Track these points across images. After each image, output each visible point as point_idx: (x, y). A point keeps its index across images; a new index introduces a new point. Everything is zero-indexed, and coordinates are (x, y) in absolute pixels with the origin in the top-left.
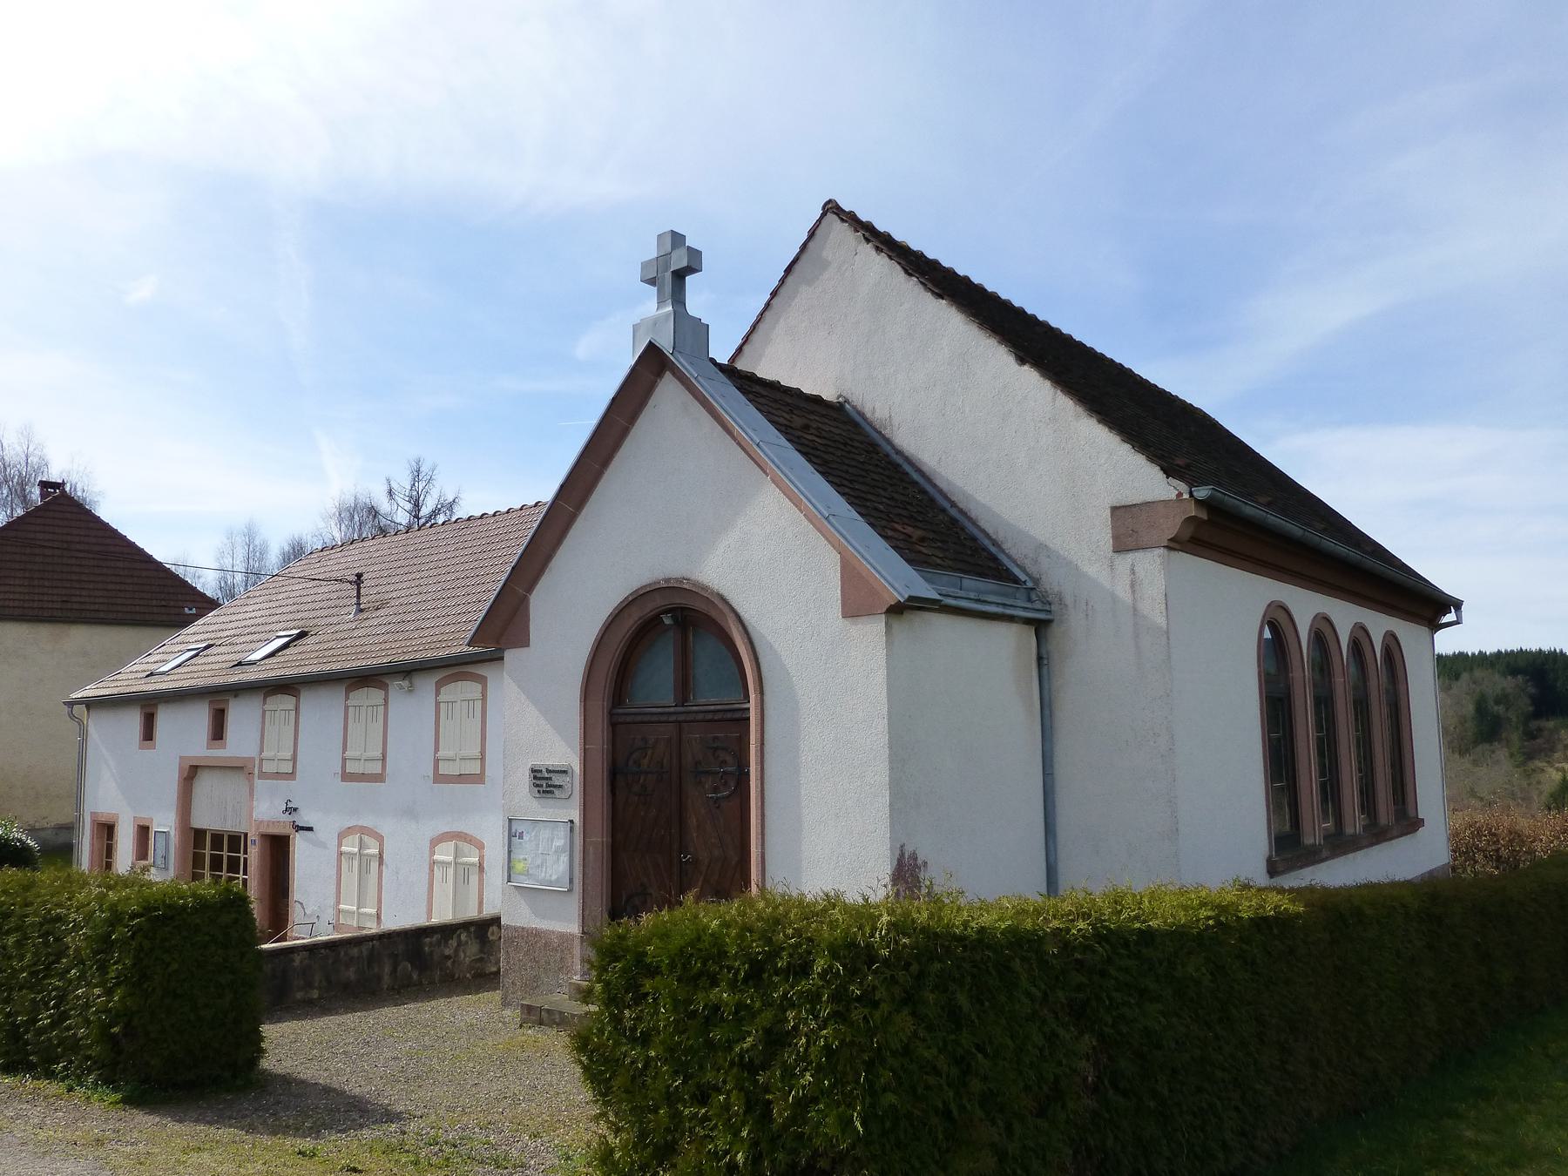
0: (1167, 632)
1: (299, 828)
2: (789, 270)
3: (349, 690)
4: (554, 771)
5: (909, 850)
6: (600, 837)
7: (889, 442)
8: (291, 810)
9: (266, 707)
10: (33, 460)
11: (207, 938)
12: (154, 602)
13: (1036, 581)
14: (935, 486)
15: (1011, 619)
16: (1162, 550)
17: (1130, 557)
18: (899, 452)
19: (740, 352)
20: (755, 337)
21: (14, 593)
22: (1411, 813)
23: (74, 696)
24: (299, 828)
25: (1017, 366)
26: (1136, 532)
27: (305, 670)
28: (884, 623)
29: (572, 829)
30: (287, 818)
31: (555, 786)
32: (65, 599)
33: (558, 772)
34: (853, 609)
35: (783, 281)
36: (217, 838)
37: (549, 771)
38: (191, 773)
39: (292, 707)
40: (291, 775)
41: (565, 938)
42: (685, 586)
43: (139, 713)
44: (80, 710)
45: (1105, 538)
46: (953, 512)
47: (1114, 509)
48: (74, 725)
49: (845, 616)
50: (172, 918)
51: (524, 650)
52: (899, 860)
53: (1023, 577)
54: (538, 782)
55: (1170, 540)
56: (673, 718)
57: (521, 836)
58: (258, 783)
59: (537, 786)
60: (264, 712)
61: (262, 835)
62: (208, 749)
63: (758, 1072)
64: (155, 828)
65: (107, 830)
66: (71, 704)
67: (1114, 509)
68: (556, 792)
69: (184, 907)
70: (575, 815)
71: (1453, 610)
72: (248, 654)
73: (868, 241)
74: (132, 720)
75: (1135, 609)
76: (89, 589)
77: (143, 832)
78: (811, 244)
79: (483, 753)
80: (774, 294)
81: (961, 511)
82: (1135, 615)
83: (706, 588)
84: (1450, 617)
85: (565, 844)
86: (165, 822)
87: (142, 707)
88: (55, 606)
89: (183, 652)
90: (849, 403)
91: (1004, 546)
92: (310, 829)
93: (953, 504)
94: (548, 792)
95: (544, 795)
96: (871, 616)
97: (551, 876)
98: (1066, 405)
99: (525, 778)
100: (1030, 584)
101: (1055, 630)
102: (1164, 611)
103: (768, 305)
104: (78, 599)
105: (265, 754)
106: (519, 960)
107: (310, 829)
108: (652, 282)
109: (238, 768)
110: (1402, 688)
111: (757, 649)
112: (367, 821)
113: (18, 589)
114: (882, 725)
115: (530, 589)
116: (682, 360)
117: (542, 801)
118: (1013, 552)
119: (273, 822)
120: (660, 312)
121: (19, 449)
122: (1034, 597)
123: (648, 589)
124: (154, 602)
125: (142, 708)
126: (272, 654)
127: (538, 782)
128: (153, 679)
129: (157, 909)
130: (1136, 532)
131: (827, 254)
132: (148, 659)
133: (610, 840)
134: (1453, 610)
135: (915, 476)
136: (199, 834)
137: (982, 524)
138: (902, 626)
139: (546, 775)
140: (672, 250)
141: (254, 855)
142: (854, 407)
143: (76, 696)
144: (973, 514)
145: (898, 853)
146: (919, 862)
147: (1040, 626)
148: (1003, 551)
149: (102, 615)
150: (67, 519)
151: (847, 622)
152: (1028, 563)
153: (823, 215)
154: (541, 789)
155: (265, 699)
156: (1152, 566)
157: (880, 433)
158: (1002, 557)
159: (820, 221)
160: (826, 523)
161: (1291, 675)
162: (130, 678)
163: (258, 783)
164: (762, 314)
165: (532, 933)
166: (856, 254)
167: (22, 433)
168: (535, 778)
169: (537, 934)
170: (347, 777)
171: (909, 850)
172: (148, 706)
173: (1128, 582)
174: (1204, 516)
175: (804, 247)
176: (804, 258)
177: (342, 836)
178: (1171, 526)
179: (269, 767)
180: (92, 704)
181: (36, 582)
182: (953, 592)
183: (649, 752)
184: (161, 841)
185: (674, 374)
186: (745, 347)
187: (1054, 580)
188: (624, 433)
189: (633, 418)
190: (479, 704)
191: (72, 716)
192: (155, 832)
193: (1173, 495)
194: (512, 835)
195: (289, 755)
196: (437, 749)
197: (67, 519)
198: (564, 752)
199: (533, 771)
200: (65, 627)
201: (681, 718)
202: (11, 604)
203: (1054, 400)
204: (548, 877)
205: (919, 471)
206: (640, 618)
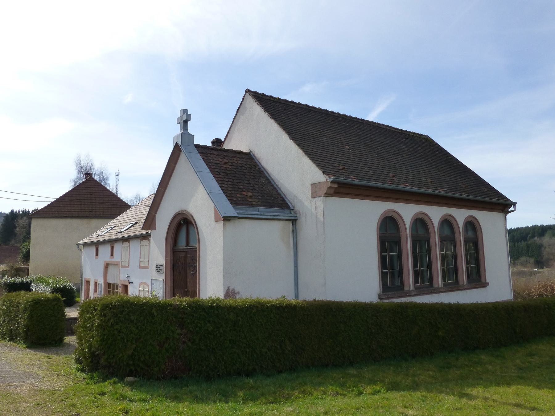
0: (324, 223)
1: (130, 283)
2: (238, 111)
3: (141, 240)
5: (231, 288)
6: (170, 284)
7: (260, 164)
8: (128, 277)
9: (141, 244)
10: (90, 164)
11: (48, 308)
12: (117, 211)
13: (294, 207)
14: (271, 177)
15: (280, 220)
16: (322, 197)
17: (315, 199)
18: (263, 167)
20: (230, 132)
21: (76, 209)
22: (483, 280)
23: (79, 243)
24: (130, 283)
27: (132, 234)
28: (223, 224)
29: (163, 282)
30: (127, 279)
31: (160, 270)
32: (91, 211)
34: (217, 220)
35: (236, 114)
36: (113, 285)
38: (107, 266)
39: (128, 246)
40: (128, 267)
43: (94, 248)
44: (81, 247)
45: (309, 193)
46: (275, 186)
47: (312, 184)
48: (79, 252)
50: (39, 302)
52: (227, 291)
53: (291, 206)
54: (157, 269)
55: (325, 194)
56: (185, 250)
58: (121, 268)
60: (140, 246)
61: (122, 285)
62: (110, 258)
64: (99, 283)
65: (88, 283)
66: (78, 245)
67: (312, 184)
69: (43, 300)
71: (513, 206)
72: (121, 229)
73: (256, 102)
74: (93, 249)
76: (98, 207)
77: (96, 283)
78: (243, 103)
79: (129, 260)
80: (234, 118)
81: (277, 185)
82: (316, 218)
83: (188, 213)
84: (512, 209)
86: (101, 281)
87: (96, 246)
88: (88, 213)
89: (108, 228)
90: (251, 152)
91: (287, 196)
92: (132, 283)
93: (275, 183)
98: (300, 152)
99: (154, 268)
100: (292, 208)
101: (298, 222)
102: (323, 216)
103: (233, 121)
104: (95, 211)
105: (123, 260)
107: (132, 283)
108: (179, 123)
109: (116, 264)
110: (479, 235)
111: (199, 231)
112: (144, 281)
113: (77, 208)
114: (222, 253)
115: (156, 213)
116: (182, 147)
118: (288, 198)
119: (125, 281)
121: (85, 162)
122: (292, 212)
124: (117, 211)
126: (127, 229)
127: (157, 269)
128: (99, 237)
129: (35, 300)
131: (247, 105)
132: (100, 231)
133: (173, 285)
134: (513, 206)
135: (267, 175)
136: (109, 284)
137: (281, 189)
138: (227, 223)
139: (159, 267)
140: (183, 114)
141: (120, 289)
142: (253, 153)
143: (80, 243)
144: (280, 186)
145: (226, 289)
146: (236, 292)
147: (294, 221)
148: (286, 198)
149: (102, 215)
150: (92, 185)
151: (216, 223)
152: (292, 201)
153: (246, 93)
155: (122, 243)
156: (319, 201)
157: (258, 161)
158: (286, 200)
159: (245, 95)
161: (401, 233)
162: (93, 238)
163: (121, 268)
164: (232, 125)
167: (86, 156)
168: (157, 267)
170: (141, 267)
171: (231, 288)
172: (97, 245)
173: (315, 207)
174: (336, 186)
175: (241, 103)
176: (241, 107)
177: (140, 285)
178: (324, 190)
179: (123, 264)
180: (84, 245)
181: (82, 206)
182: (250, 213)
183: (180, 260)
184: (100, 286)
186: (228, 135)
187: (298, 207)
190: (128, 247)
191: (79, 249)
192: (99, 284)
194: (152, 284)
195: (127, 260)
196: (140, 259)
197: (92, 185)
198: (162, 261)
199: (156, 265)
200: (91, 220)
201: (186, 250)
202: (75, 213)
205: (267, 173)
206: (178, 221)
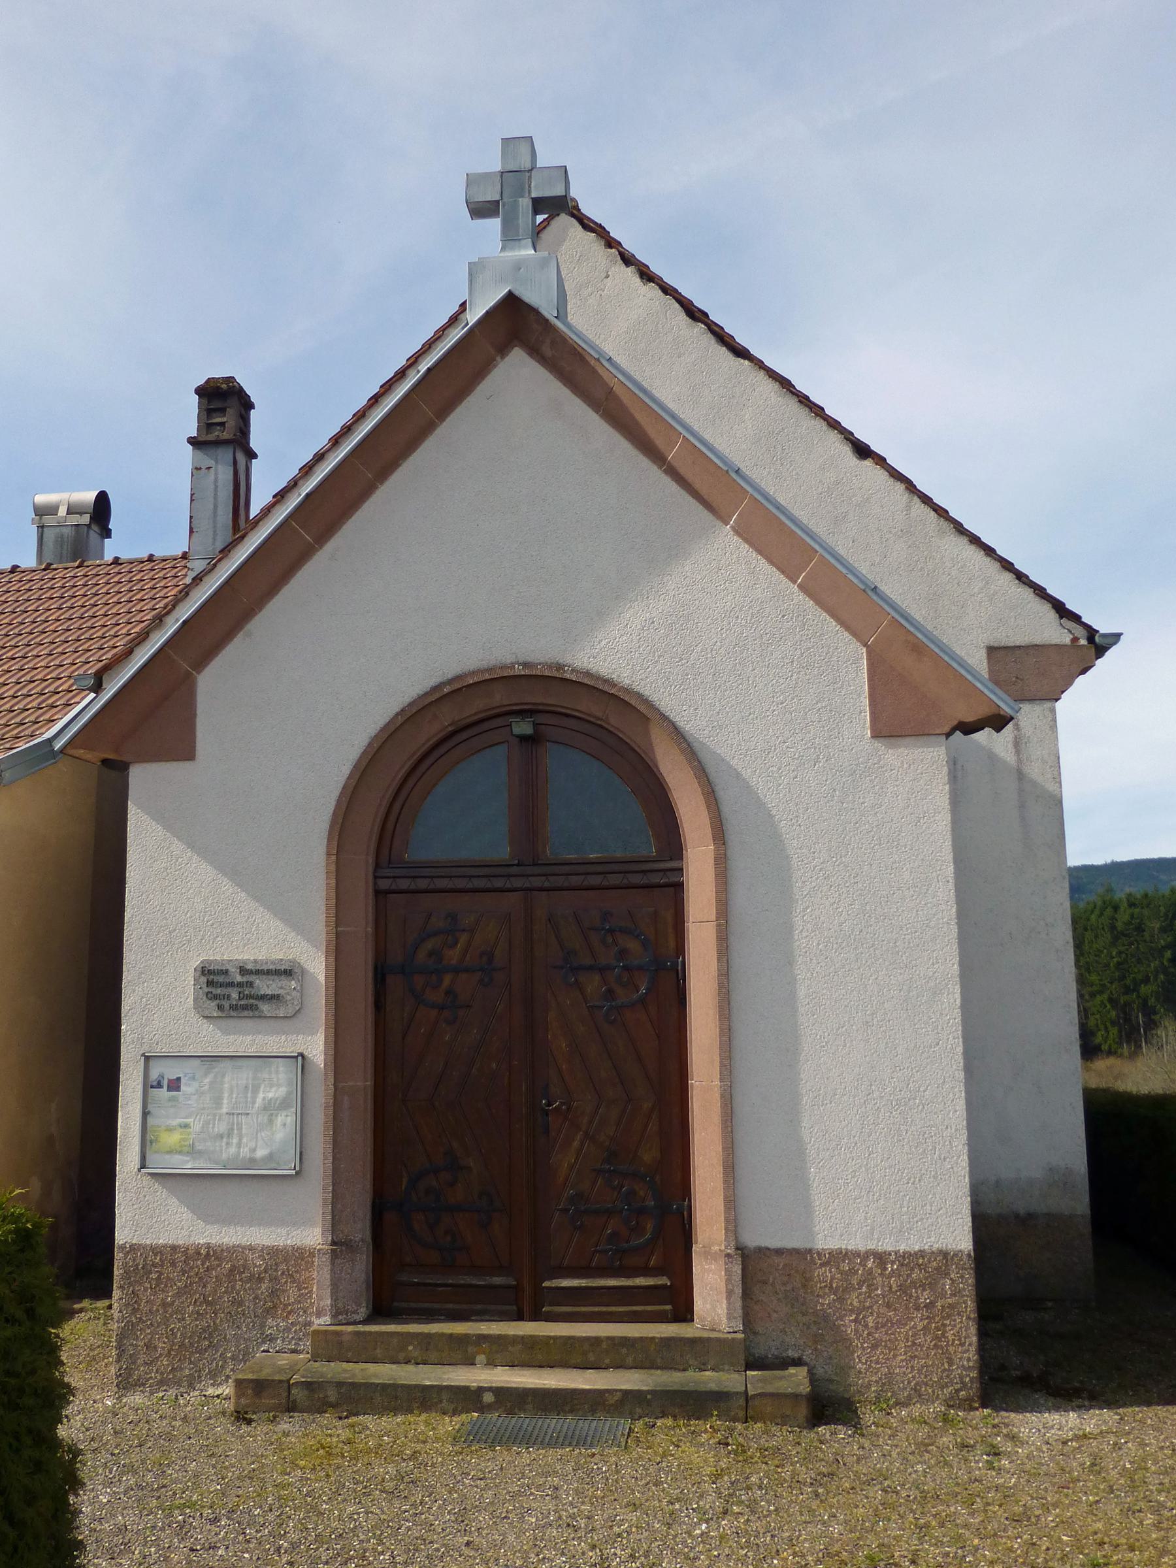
4: (258, 972)
6: (362, 1081)
19: (402, 377)
25: (855, 459)
26: (1022, 680)
31: (263, 998)
33: (268, 972)
37: (243, 971)
41: (300, 1256)
42: (568, 676)
49: (877, 735)
51: (187, 765)
57: (175, 1085)
59: (215, 997)
63: (59, 1458)
68: (265, 1008)
70: (316, 1047)
75: (1020, 775)
85: (289, 1093)
94: (245, 1008)
95: (233, 1013)
96: (920, 737)
97: (254, 1150)
99: (188, 986)
106: (164, 1304)
117: (224, 1023)
120: (502, 254)
123: (487, 677)
125: (906, 487)
130: (1022, 680)
139: (239, 979)
151: (877, 744)
154: (226, 1004)
160: (875, 598)
165: (199, 1253)
166: (607, 277)
168: (210, 983)
169: (212, 1255)
185: (534, 351)
188: (427, 429)
189: (444, 410)
193: (1067, 639)
203: (908, 507)
204: (245, 1152)
